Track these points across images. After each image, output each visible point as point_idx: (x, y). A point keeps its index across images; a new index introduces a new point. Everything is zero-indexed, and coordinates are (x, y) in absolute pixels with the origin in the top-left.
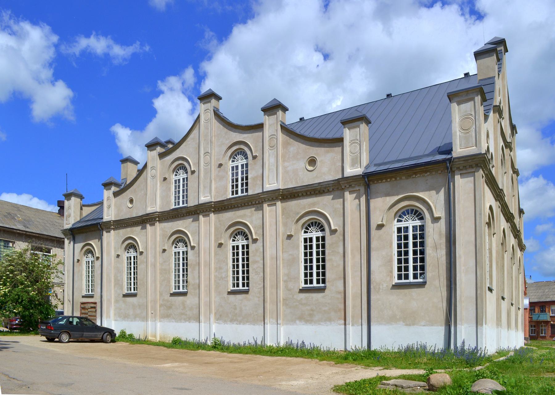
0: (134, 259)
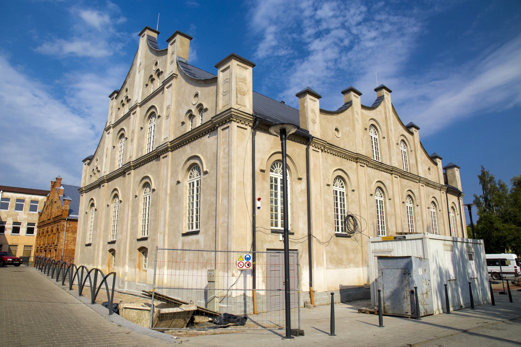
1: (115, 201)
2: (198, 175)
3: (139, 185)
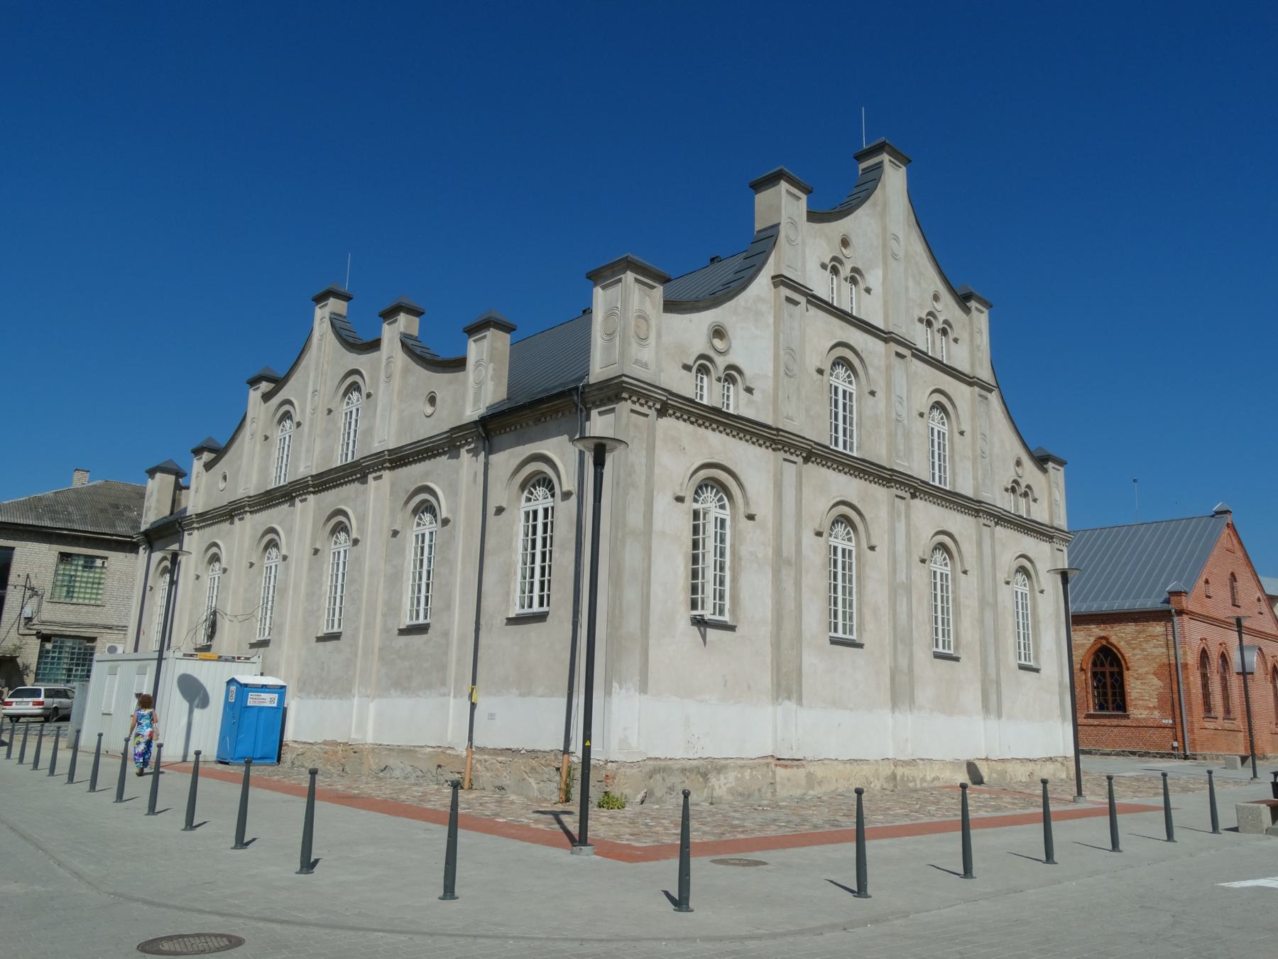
0: (546, 517)
1: (270, 553)
2: (547, 498)
3: (204, 557)
